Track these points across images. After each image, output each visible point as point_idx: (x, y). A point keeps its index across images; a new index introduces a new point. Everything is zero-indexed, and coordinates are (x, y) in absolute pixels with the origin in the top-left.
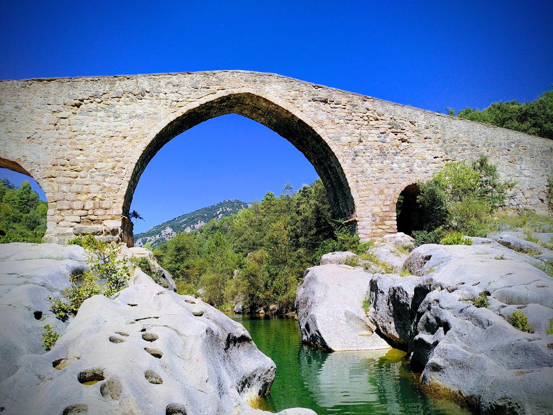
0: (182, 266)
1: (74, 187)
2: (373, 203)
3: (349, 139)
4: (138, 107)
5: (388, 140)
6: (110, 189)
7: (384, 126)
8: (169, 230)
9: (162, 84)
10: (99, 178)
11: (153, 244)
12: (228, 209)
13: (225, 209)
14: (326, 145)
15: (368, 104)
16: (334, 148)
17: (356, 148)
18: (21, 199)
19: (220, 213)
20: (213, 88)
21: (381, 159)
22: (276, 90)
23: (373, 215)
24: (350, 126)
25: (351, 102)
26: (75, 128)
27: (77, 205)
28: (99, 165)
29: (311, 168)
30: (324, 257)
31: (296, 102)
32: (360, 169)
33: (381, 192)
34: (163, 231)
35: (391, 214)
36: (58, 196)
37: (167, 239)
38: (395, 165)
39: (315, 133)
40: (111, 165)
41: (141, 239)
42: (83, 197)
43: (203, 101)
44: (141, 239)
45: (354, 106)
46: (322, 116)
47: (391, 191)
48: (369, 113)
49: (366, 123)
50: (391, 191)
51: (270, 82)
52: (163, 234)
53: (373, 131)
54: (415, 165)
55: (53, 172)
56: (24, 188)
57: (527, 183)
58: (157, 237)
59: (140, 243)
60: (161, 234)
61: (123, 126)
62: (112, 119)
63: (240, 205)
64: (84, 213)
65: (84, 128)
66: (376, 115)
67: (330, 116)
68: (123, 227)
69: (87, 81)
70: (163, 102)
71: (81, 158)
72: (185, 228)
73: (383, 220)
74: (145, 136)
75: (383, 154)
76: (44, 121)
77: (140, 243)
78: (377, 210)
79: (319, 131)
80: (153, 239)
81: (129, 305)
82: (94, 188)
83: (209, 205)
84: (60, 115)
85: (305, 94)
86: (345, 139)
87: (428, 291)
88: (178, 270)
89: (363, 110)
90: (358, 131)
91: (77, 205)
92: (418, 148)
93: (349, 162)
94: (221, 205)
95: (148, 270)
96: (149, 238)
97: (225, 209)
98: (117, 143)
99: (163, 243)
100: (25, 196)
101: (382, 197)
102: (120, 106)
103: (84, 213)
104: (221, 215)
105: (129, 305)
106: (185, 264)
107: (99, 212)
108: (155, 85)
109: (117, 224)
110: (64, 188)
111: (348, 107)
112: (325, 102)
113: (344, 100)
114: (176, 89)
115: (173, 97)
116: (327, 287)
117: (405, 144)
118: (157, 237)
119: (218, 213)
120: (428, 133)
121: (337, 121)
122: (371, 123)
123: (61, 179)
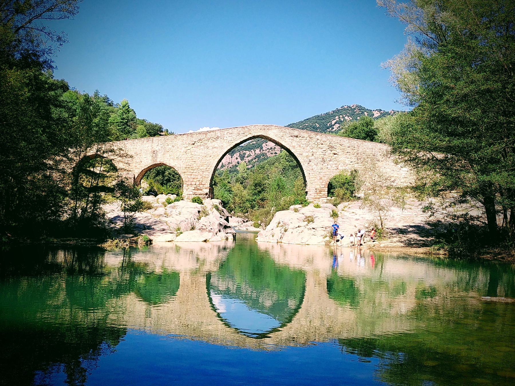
0: (258, 198)
1: (192, 176)
2: (316, 183)
3: (307, 154)
4: (216, 144)
5: (327, 154)
6: (205, 177)
7: (325, 147)
9: (225, 133)
10: (201, 173)
11: (252, 160)
12: (346, 118)
15: (318, 137)
17: (310, 158)
18: (122, 119)
19: (336, 123)
20: (246, 134)
21: (322, 163)
23: (316, 189)
24: (308, 148)
26: (193, 153)
27: (193, 183)
28: (201, 168)
32: (311, 168)
33: (321, 178)
34: (264, 145)
35: (324, 189)
36: (187, 180)
37: (269, 155)
38: (329, 166)
40: (205, 167)
41: (238, 154)
42: (195, 180)
44: (238, 154)
45: (311, 138)
47: (325, 178)
48: (318, 141)
49: (316, 146)
50: (325, 178)
52: (264, 149)
53: (320, 150)
54: (340, 166)
55: (185, 171)
56: (124, 107)
57: (403, 174)
58: (258, 151)
59: (237, 158)
60: (262, 148)
61: (210, 152)
63: (363, 113)
64: (196, 186)
65: (196, 153)
66: (322, 142)
68: (209, 192)
70: (226, 141)
71: (195, 165)
73: (320, 191)
74: (218, 156)
75: (324, 161)
76: (182, 151)
77: (237, 158)
78: (318, 187)
80: (252, 153)
82: (199, 177)
83: (322, 112)
84: (188, 148)
86: (305, 154)
87: (419, 230)
88: (255, 201)
89: (315, 140)
90: (311, 150)
91: (193, 183)
92: (342, 157)
93: (306, 164)
94: (338, 112)
95: (218, 209)
96: (248, 153)
98: (207, 159)
99: (265, 159)
100: (125, 116)
101: (321, 181)
102: (210, 144)
103: (196, 186)
104: (337, 125)
106: (260, 197)
107: (201, 186)
109: (207, 191)
110: (189, 177)
111: (308, 138)
112: (297, 137)
113: (306, 135)
114: (231, 135)
115: (229, 139)
117: (335, 155)
120: (349, 150)
122: (319, 146)
123: (188, 173)
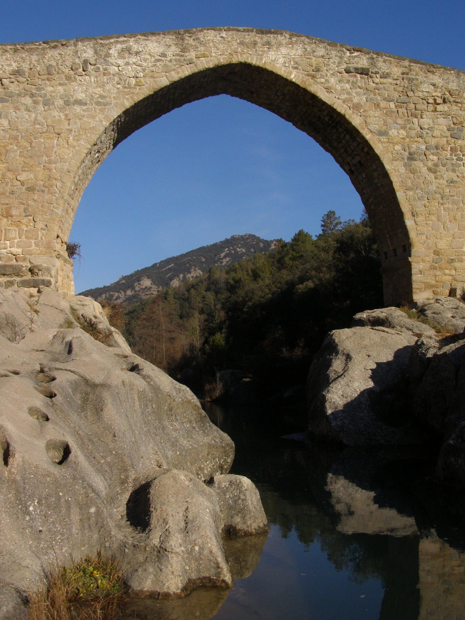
8: (147, 282)
13: (234, 249)
14: (365, 142)
16: (378, 149)
19: (225, 257)
22: (283, 57)
25: (407, 74)
29: (344, 180)
30: (358, 316)
31: (318, 75)
39: (349, 123)
43: (176, 77)
46: (358, 98)
51: (280, 45)
52: (137, 289)
53: (441, 120)
58: (129, 293)
62: (41, 107)
67: (372, 96)
69: (6, 51)
72: (171, 279)
79: (356, 121)
81: (37, 351)
85: (334, 63)
97: (234, 249)
102: (55, 89)
105: (37, 351)
108: (103, 54)
112: (364, 72)
113: (396, 71)
116: (348, 357)
118: (129, 293)
119: (223, 255)
121: (383, 104)
